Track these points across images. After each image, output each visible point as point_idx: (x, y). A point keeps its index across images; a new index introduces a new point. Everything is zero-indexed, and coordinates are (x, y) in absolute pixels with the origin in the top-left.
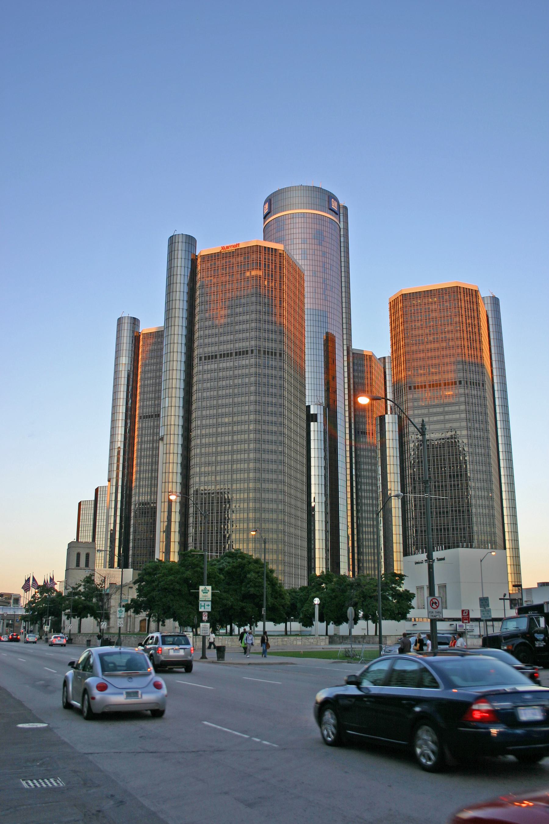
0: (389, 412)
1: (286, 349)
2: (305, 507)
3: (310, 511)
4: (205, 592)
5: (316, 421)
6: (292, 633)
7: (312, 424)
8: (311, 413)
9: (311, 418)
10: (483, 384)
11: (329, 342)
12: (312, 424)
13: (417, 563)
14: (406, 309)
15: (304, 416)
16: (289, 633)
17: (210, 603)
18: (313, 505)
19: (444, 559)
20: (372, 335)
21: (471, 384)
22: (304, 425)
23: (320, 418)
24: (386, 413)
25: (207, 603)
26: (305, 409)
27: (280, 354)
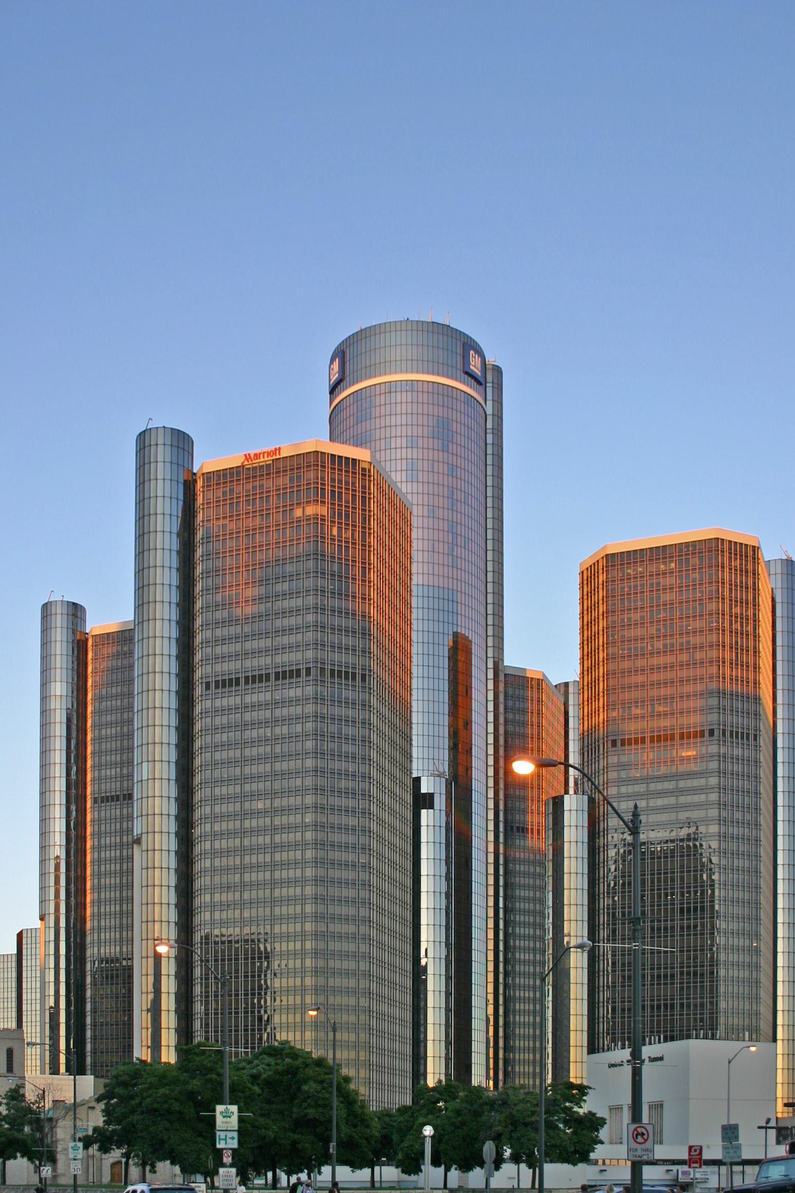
0: (571, 791)
1: (374, 666)
2: (409, 966)
3: (419, 972)
4: (227, 1115)
5: (431, 806)
6: (384, 1185)
7: (424, 812)
8: (424, 790)
9: (423, 801)
10: (755, 736)
11: (459, 652)
12: (424, 812)
13: (612, 1066)
14: (614, 585)
15: (409, 798)
16: (377, 1185)
17: (235, 1135)
18: (423, 962)
19: (661, 1059)
20: (544, 640)
21: (732, 736)
22: (409, 815)
23: (440, 802)
24: (567, 792)
25: (230, 1134)
26: (410, 783)
27: (363, 677)
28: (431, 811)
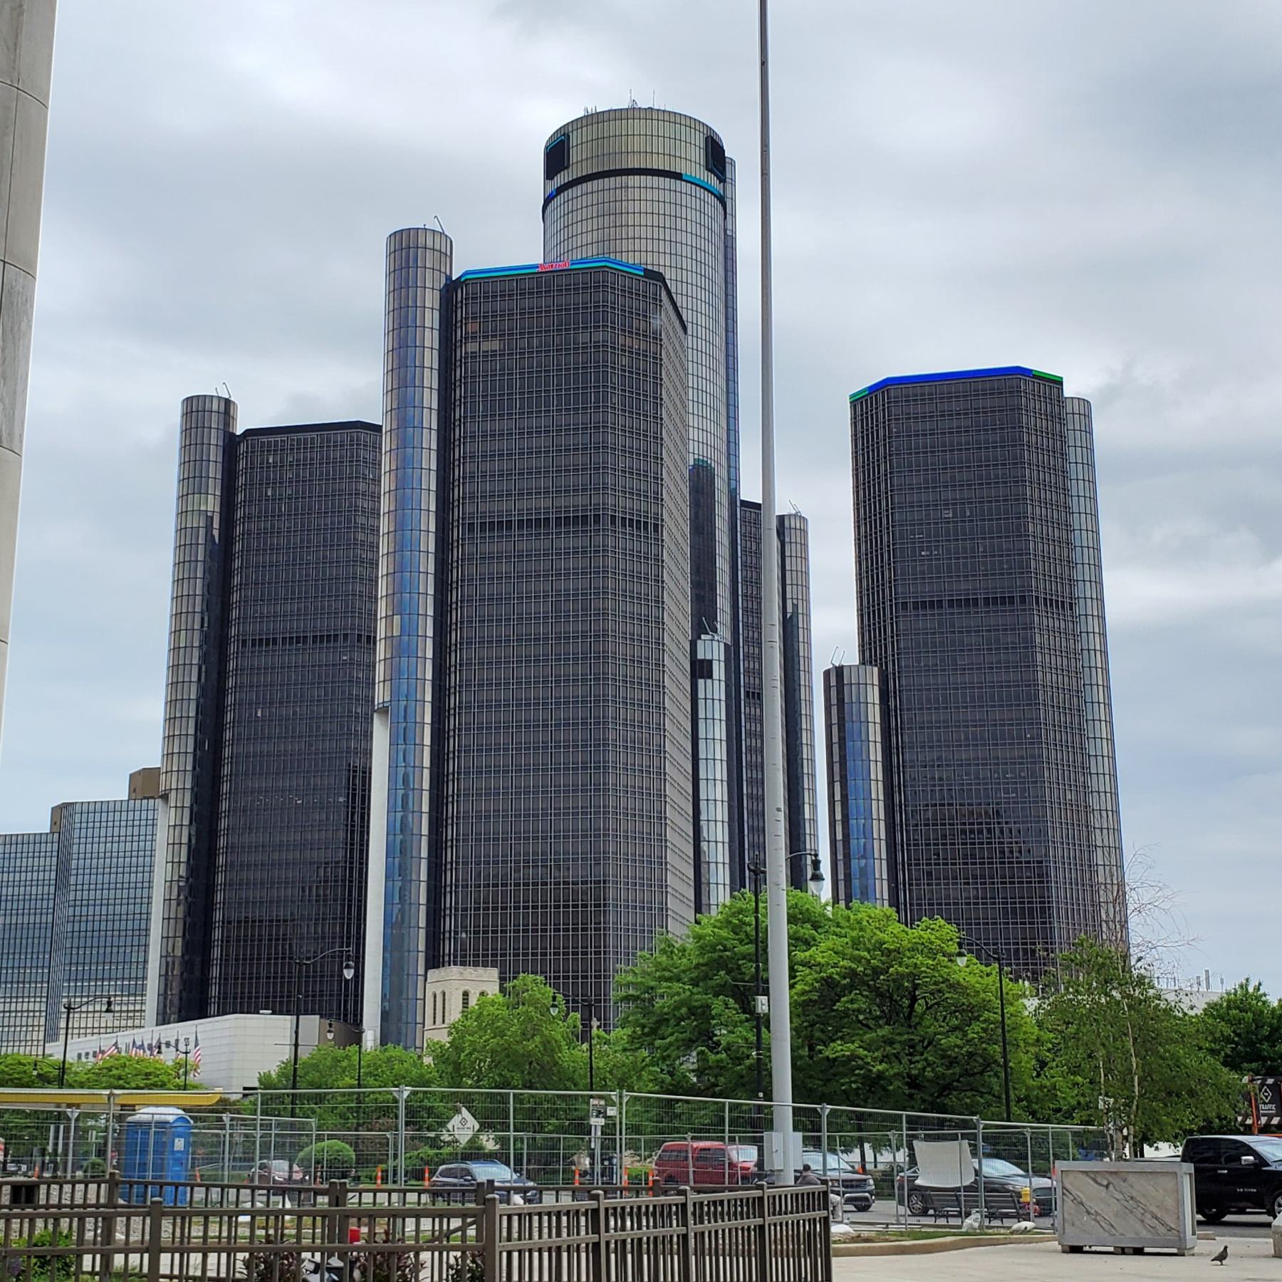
8: (700, 656)
12: (701, 682)
23: (719, 671)
28: (709, 681)
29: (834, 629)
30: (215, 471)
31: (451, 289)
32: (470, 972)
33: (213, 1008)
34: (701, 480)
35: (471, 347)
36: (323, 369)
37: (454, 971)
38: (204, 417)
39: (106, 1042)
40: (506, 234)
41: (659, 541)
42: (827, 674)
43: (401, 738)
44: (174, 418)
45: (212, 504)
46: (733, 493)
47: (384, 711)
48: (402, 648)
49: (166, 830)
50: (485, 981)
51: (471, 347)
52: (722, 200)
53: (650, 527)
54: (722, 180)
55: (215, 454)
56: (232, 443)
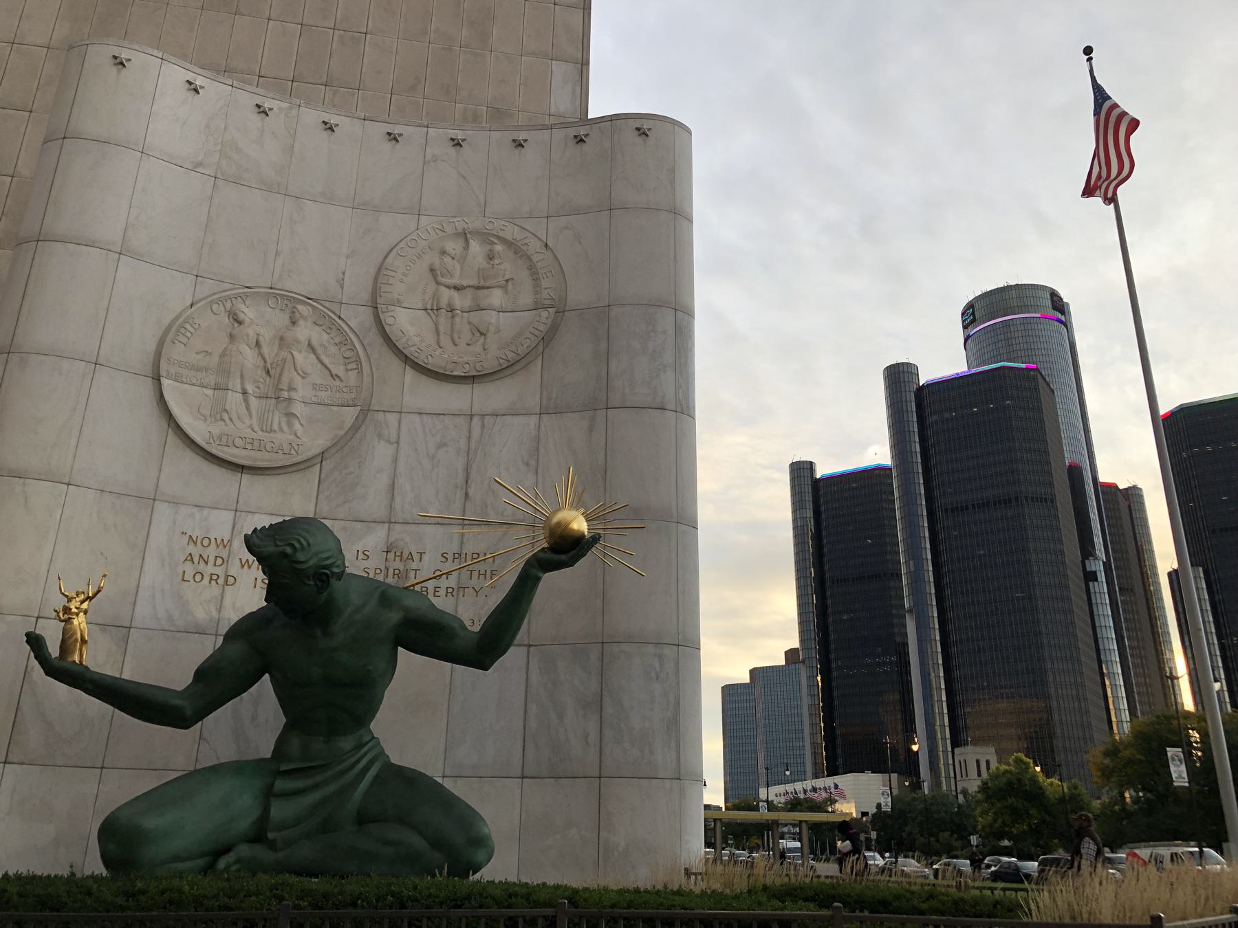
23: (1102, 577)
29: (1165, 553)
30: (809, 497)
31: (921, 389)
32: (978, 749)
33: (841, 770)
34: (1075, 474)
35: (935, 418)
36: (861, 440)
37: (970, 748)
38: (801, 472)
39: (790, 788)
40: (943, 357)
41: (1056, 508)
42: (1170, 574)
43: (922, 627)
44: (786, 478)
45: (809, 513)
46: (1095, 479)
47: (910, 611)
48: (917, 579)
49: (811, 680)
50: (988, 754)
51: (935, 418)
52: (1066, 326)
53: (1049, 501)
54: (1063, 313)
55: (809, 489)
56: (816, 483)
